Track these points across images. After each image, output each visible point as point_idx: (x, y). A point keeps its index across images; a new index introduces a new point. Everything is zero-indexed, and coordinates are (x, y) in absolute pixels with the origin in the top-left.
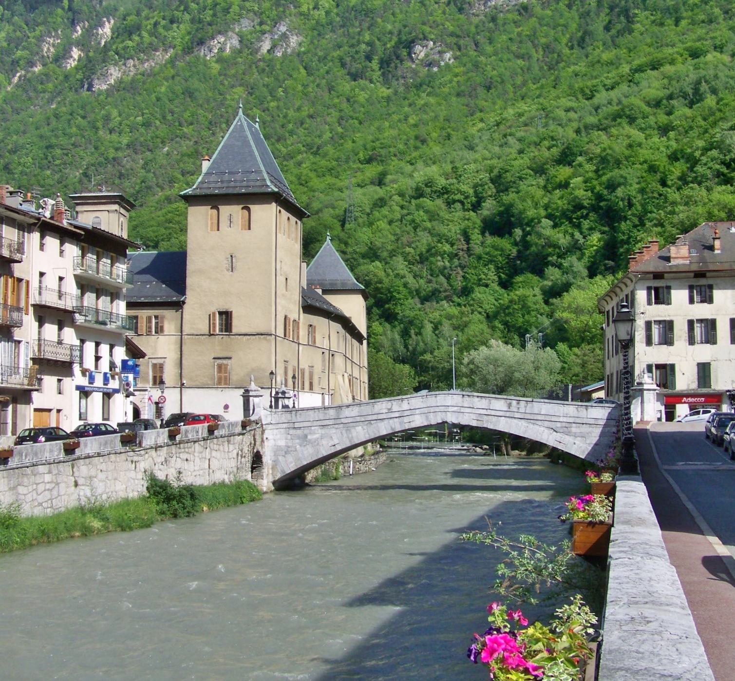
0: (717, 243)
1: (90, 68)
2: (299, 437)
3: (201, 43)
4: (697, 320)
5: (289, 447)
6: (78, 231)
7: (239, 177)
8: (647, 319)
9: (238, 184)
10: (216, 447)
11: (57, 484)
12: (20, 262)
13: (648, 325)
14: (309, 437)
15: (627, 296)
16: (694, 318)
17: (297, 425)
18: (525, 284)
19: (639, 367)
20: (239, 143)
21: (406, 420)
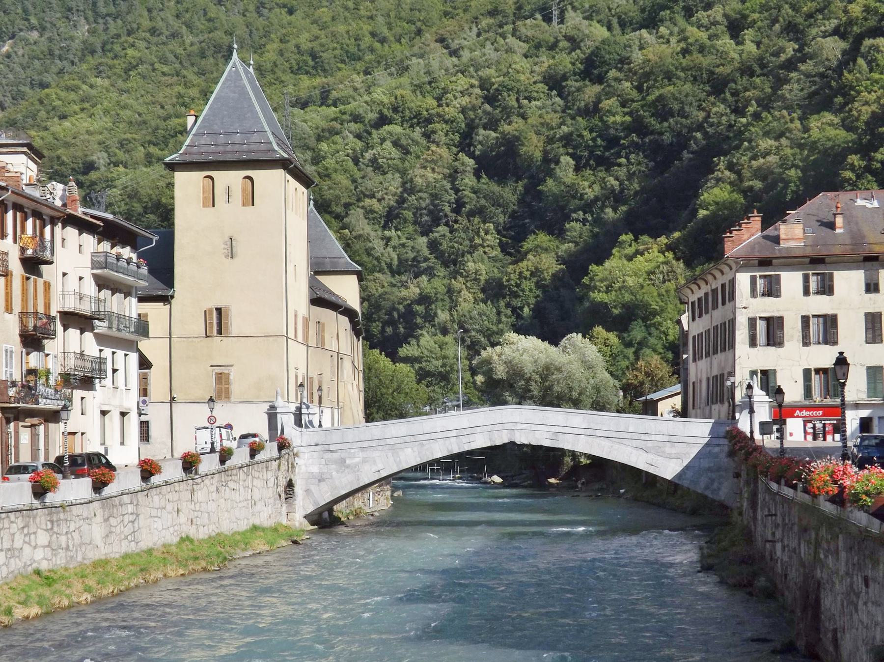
0: (839, 221)
2: (335, 462)
4: (814, 316)
5: (323, 473)
6: (95, 221)
7: (238, 138)
8: (751, 315)
9: (237, 148)
10: (256, 474)
11: (138, 515)
12: (51, 263)
13: (752, 322)
14: (348, 462)
15: (723, 286)
16: (810, 314)
17: (332, 448)
18: (538, 249)
19: (741, 376)
20: (236, 95)
21: (464, 439)
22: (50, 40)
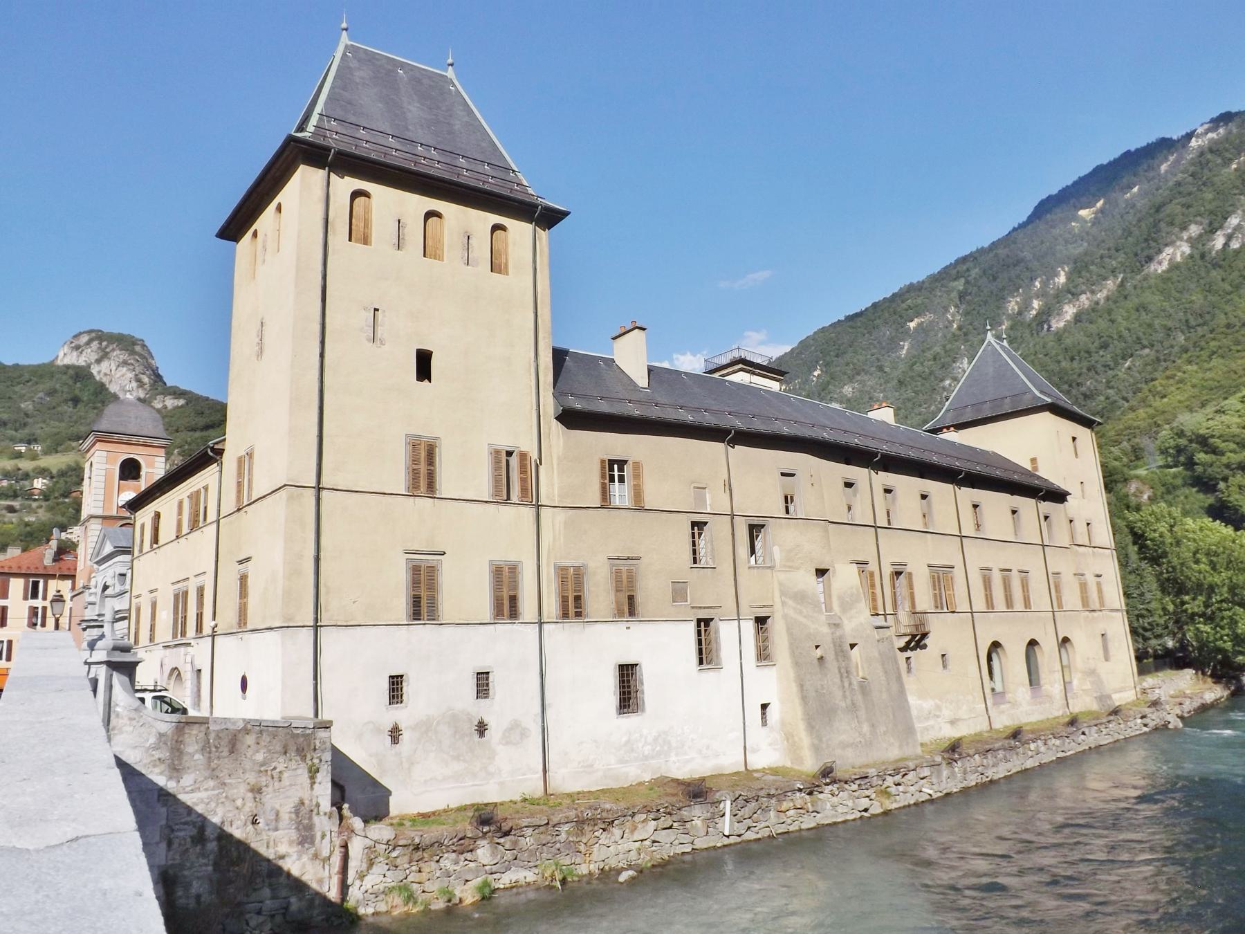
1: (1044, 317)
3: (1150, 259)
22: (1157, 351)
